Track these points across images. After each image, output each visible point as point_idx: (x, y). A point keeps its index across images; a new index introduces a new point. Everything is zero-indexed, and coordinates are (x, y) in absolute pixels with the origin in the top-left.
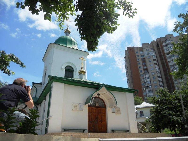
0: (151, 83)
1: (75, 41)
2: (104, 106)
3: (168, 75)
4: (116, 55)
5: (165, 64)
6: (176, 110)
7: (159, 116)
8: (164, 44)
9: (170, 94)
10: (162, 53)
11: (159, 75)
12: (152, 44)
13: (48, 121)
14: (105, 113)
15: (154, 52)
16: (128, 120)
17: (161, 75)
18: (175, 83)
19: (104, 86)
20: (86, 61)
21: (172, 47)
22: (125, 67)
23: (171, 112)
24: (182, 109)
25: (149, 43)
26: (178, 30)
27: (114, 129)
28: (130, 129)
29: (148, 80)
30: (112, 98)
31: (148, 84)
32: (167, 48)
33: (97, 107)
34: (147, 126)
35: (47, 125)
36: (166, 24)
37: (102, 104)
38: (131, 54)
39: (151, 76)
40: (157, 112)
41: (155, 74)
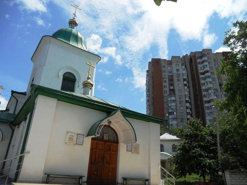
0: (176, 109)
1: (83, 38)
2: (116, 140)
3: (199, 101)
4: (135, 68)
5: (197, 87)
6: (209, 149)
7: (187, 157)
8: (199, 60)
9: (203, 127)
10: (195, 72)
11: (187, 99)
12: (184, 58)
13: (21, 159)
14: (116, 151)
15: (186, 69)
16: (149, 163)
17: (190, 99)
18: (206, 112)
19: (119, 110)
20: (95, 68)
21: (208, 66)
22: (146, 84)
23: (202, 153)
24: (217, 149)
25: (181, 57)
26: (229, 43)
27: (127, 178)
28: (150, 178)
29: (173, 104)
30: (130, 130)
31: (173, 109)
32: (202, 66)
33: (105, 141)
34: (166, 166)
35: (19, 167)
36: (202, 38)
37: (113, 137)
38: (156, 68)
39: (178, 100)
40: (184, 150)
41: (183, 97)
